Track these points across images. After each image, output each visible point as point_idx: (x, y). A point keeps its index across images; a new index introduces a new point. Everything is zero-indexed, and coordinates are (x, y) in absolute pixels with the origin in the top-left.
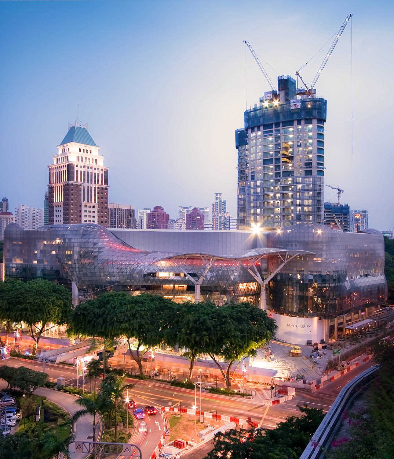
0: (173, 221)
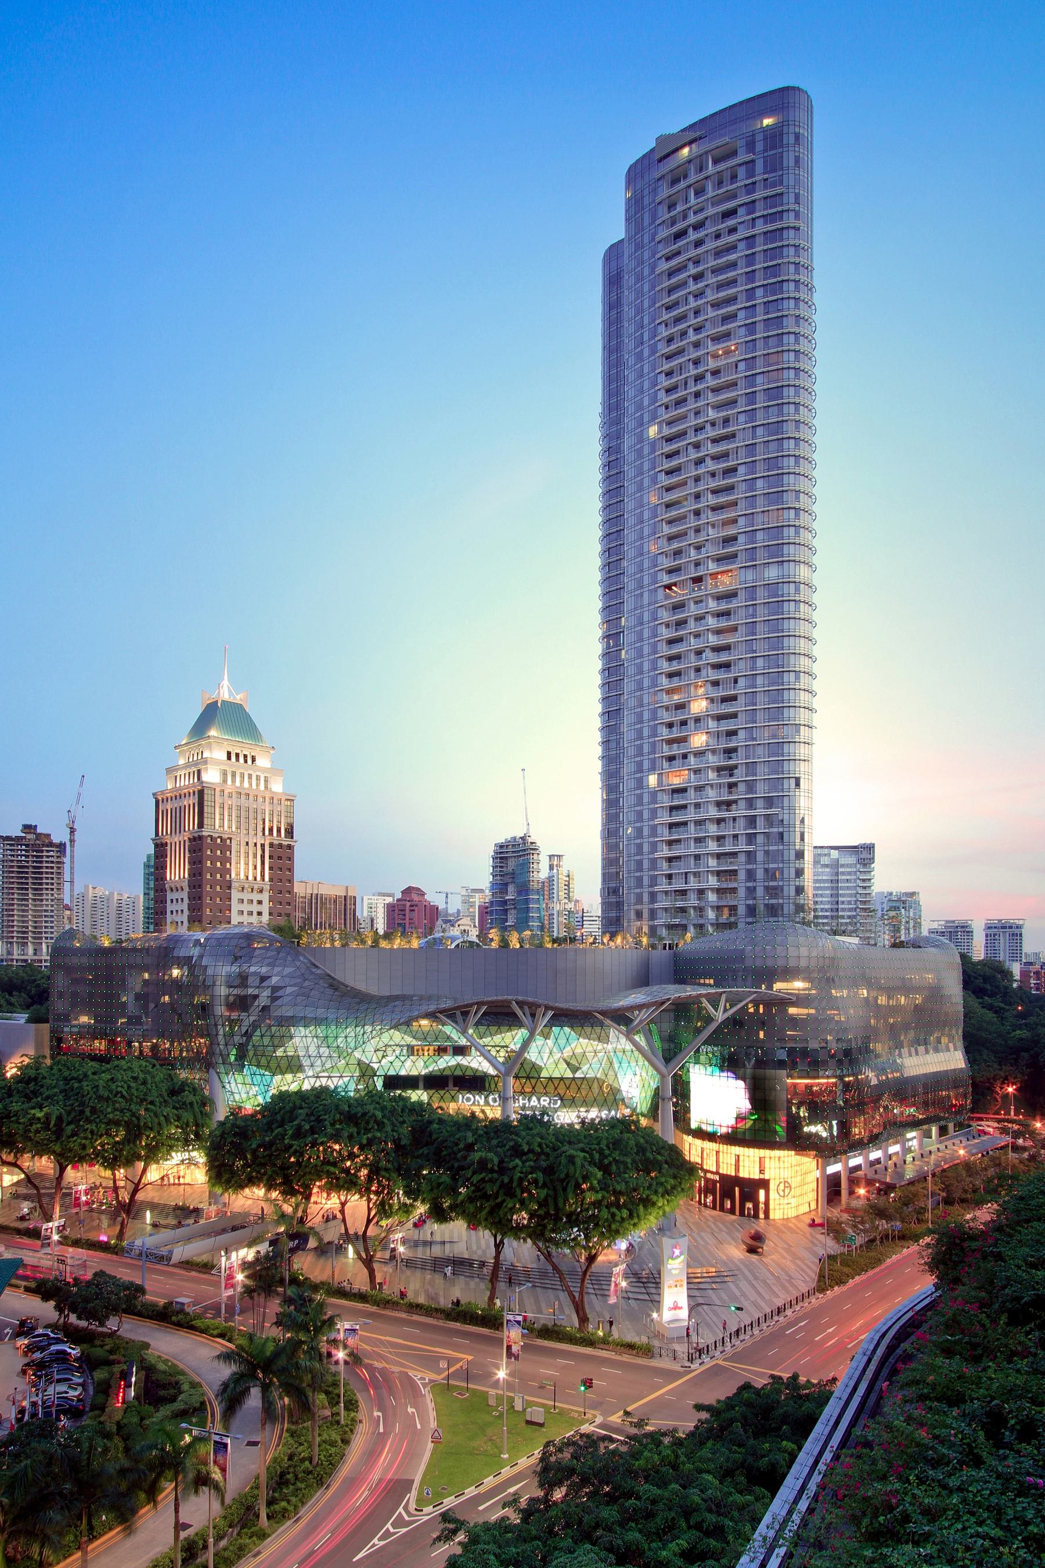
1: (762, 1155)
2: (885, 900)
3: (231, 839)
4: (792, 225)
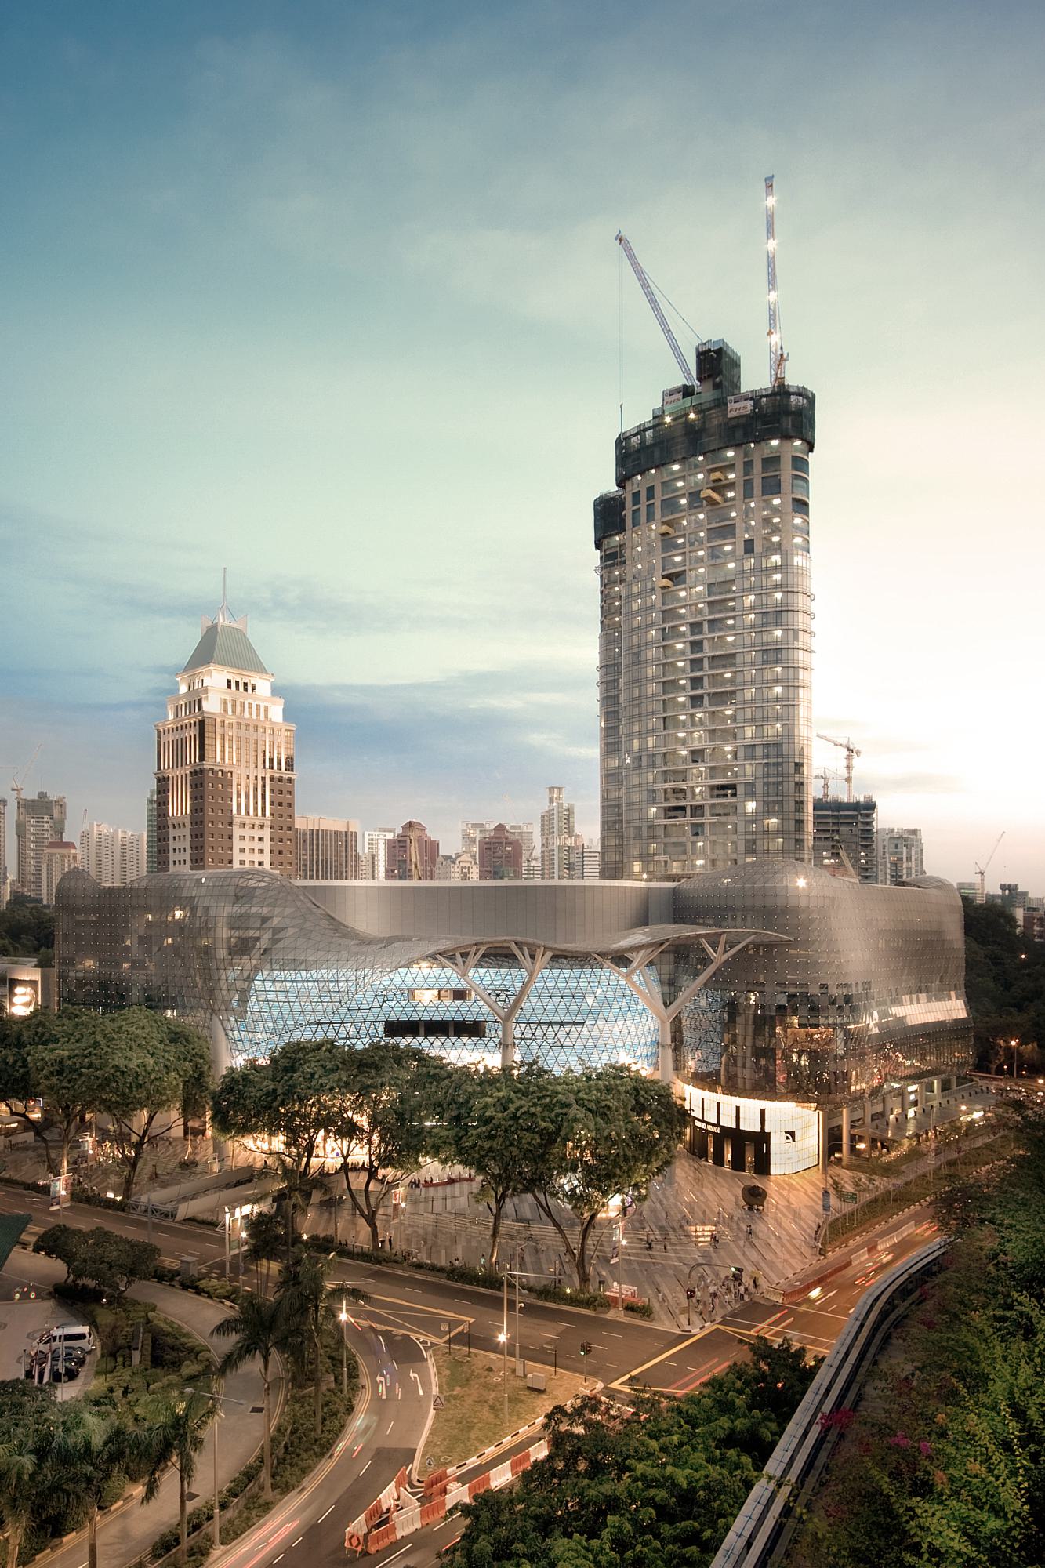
0: (447, 858)
3: (231, 772)
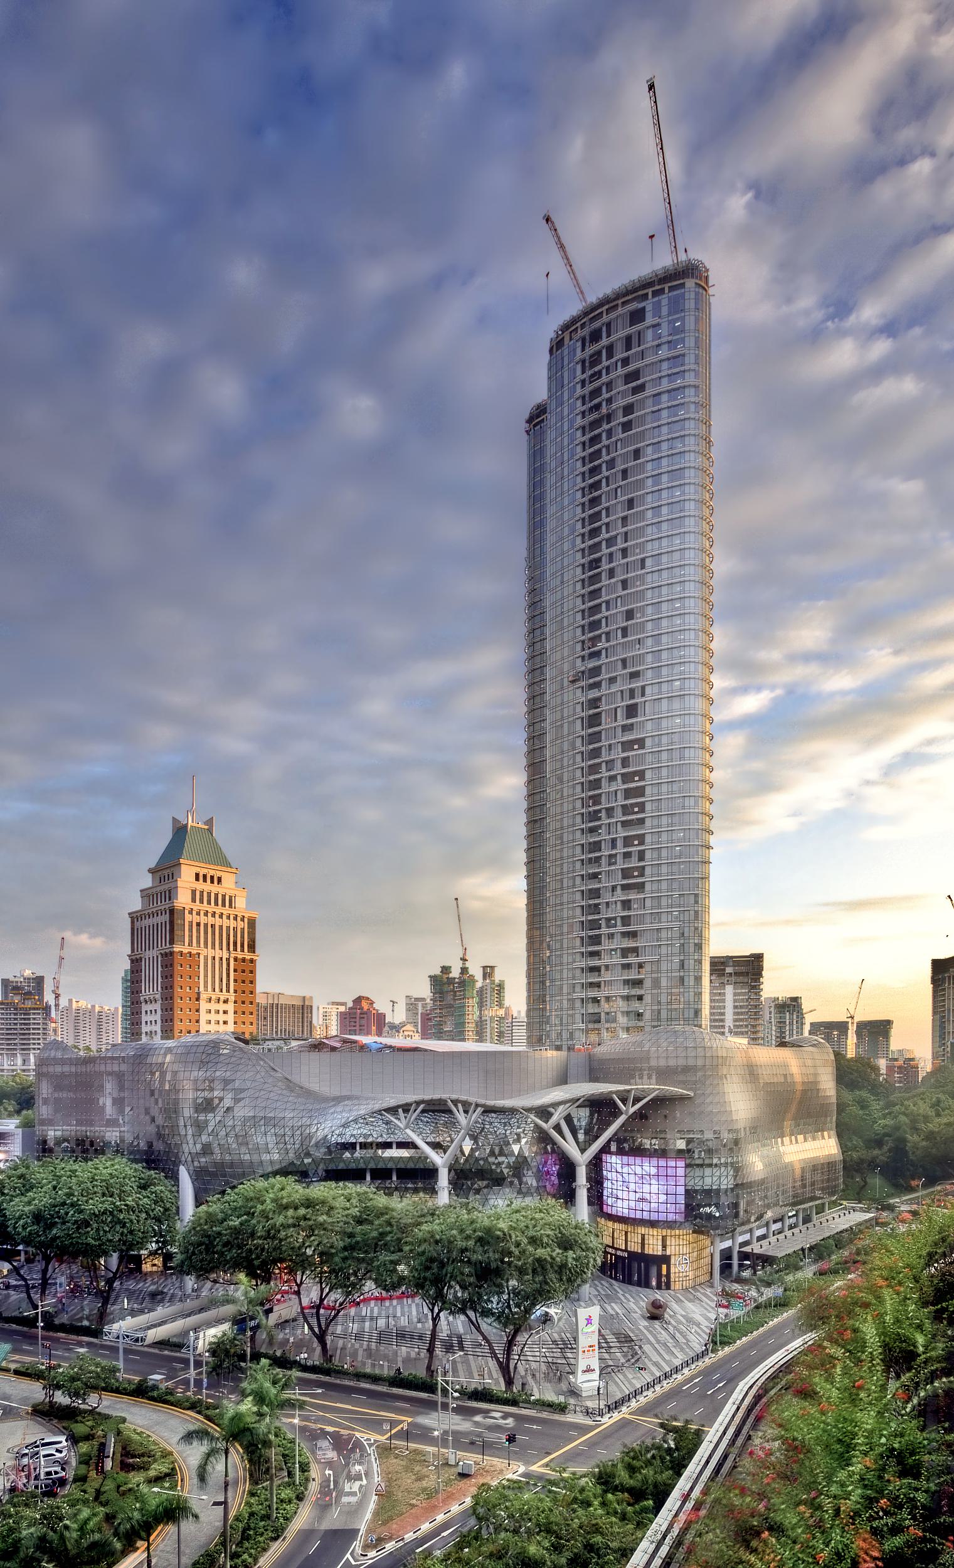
1: (664, 1234)
2: (773, 1005)
4: (692, 383)
